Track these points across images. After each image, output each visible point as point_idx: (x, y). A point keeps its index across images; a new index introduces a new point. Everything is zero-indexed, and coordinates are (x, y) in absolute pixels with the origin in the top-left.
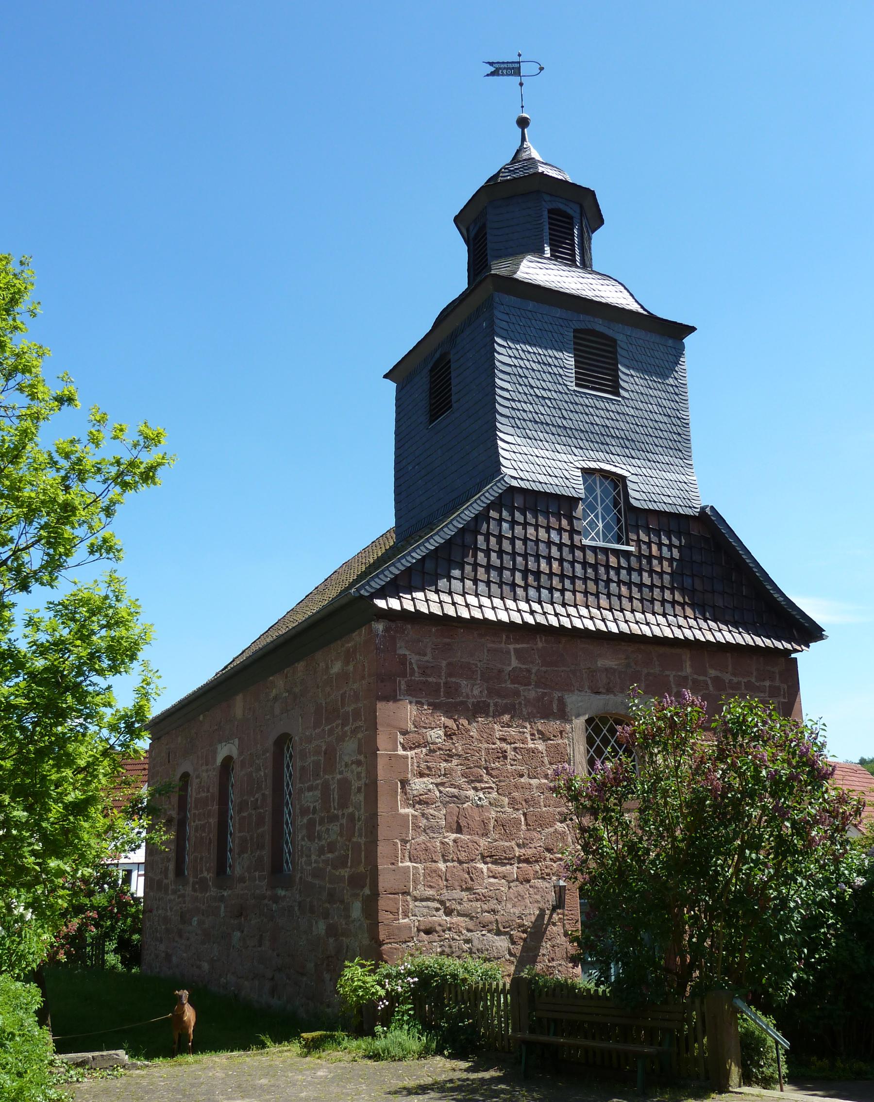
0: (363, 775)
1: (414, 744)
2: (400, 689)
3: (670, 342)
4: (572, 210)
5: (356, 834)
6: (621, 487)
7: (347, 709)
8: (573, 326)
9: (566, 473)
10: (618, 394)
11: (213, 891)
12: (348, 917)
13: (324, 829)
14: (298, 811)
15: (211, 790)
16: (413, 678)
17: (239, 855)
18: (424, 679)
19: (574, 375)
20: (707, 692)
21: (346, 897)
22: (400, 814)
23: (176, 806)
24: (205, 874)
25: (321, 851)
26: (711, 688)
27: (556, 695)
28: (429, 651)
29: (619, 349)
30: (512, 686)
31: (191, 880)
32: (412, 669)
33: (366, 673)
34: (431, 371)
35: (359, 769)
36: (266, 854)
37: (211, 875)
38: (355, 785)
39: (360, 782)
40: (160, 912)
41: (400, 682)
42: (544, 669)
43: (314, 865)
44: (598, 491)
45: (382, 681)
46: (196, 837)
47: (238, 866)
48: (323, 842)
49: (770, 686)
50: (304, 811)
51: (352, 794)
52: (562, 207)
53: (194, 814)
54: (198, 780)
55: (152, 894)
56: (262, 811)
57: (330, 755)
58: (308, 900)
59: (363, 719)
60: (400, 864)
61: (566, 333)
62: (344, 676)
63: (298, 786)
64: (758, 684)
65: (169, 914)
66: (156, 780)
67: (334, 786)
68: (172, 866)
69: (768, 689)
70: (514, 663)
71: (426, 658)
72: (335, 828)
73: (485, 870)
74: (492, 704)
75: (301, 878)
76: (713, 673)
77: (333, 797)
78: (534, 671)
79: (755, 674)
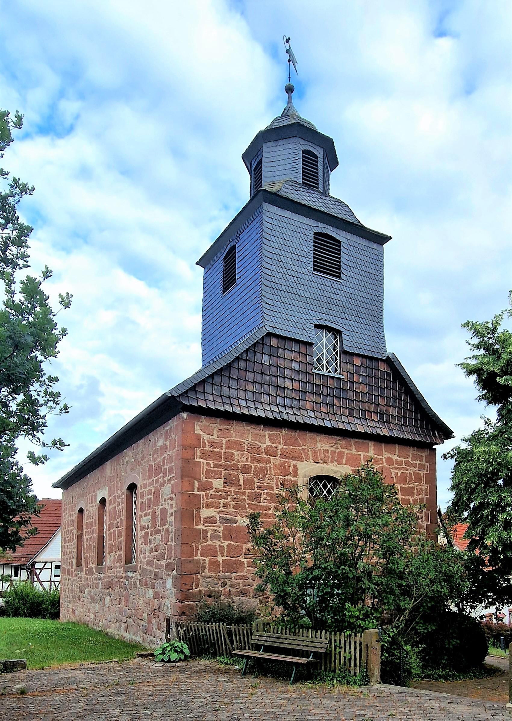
0: (174, 506)
1: (204, 488)
2: (197, 455)
3: (375, 246)
4: (319, 152)
5: (170, 540)
6: (338, 338)
7: (166, 467)
8: (314, 230)
9: (304, 326)
10: (339, 277)
11: (96, 575)
12: (165, 587)
13: (153, 538)
14: (139, 528)
15: (94, 518)
16: (205, 448)
17: (109, 554)
18: (212, 449)
19: (313, 263)
20: (382, 465)
21: (164, 577)
22: (196, 529)
23: (76, 527)
24: (91, 565)
25: (151, 551)
26: (385, 464)
27: (293, 463)
28: (215, 432)
29: (342, 248)
30: (266, 456)
31: (84, 569)
32: (204, 443)
33: (176, 445)
34: (224, 259)
35: (172, 502)
36: (122, 553)
37: (94, 565)
38: (169, 512)
39: (172, 510)
40: (69, 586)
41: (196, 450)
42: (285, 447)
43: (147, 559)
44: (324, 339)
45: (185, 450)
46: (87, 544)
47: (108, 560)
48: (152, 546)
49: (419, 464)
50: (143, 528)
51: (168, 517)
52: (312, 150)
53: (86, 531)
54: (88, 512)
55: (65, 577)
56: (121, 529)
57: (156, 494)
58: (144, 578)
59: (174, 472)
60: (195, 558)
61: (309, 234)
62: (164, 448)
63: (140, 513)
64: (412, 462)
65: (74, 587)
66: (66, 513)
67: (158, 513)
68: (75, 561)
69: (418, 465)
70: (268, 443)
71: (213, 437)
72: (158, 537)
73: (245, 563)
74: (253, 467)
75: (140, 566)
76: (387, 455)
77: (158, 520)
78: (279, 448)
79: (411, 456)
